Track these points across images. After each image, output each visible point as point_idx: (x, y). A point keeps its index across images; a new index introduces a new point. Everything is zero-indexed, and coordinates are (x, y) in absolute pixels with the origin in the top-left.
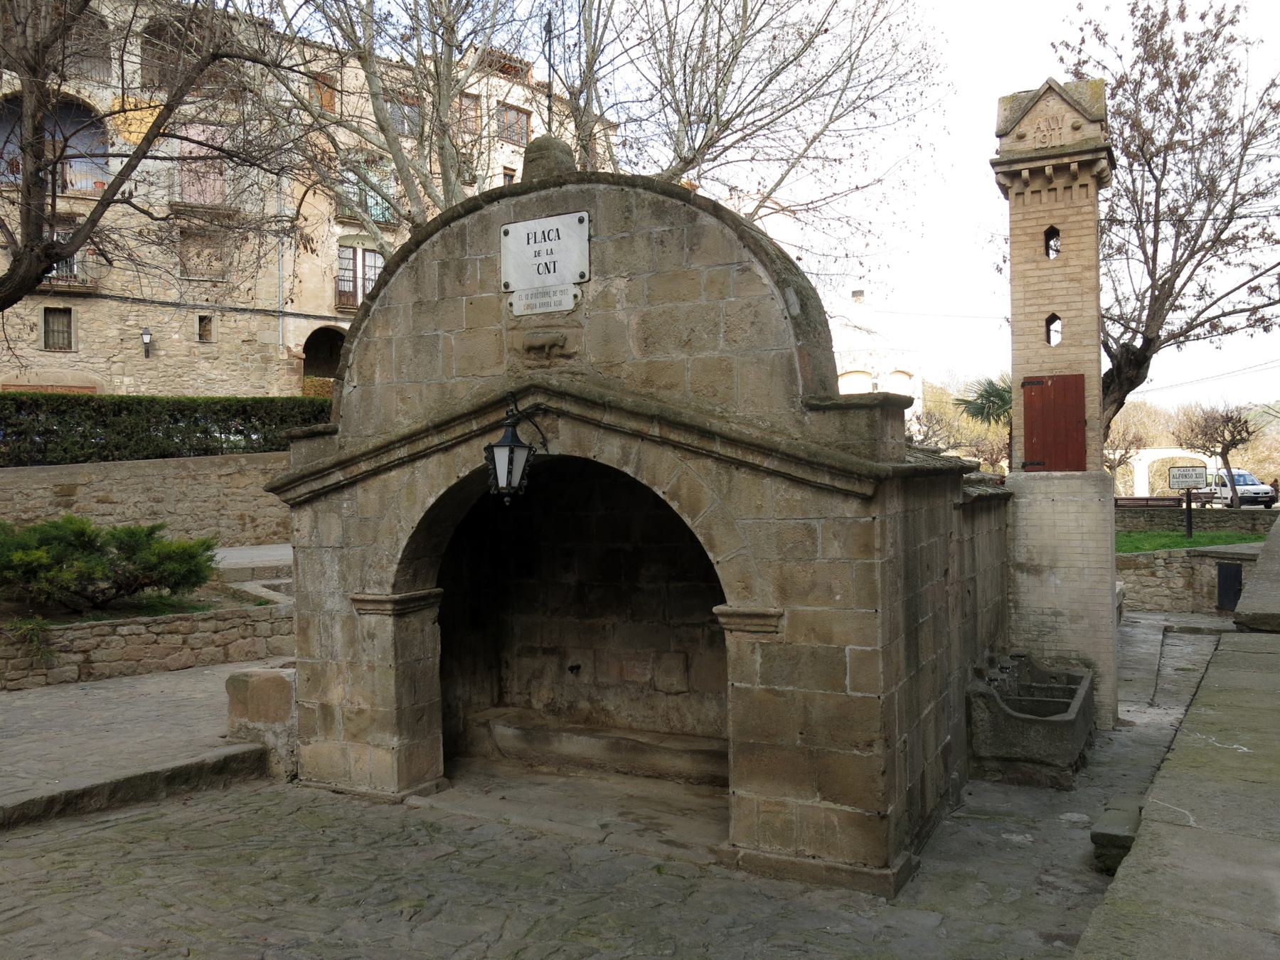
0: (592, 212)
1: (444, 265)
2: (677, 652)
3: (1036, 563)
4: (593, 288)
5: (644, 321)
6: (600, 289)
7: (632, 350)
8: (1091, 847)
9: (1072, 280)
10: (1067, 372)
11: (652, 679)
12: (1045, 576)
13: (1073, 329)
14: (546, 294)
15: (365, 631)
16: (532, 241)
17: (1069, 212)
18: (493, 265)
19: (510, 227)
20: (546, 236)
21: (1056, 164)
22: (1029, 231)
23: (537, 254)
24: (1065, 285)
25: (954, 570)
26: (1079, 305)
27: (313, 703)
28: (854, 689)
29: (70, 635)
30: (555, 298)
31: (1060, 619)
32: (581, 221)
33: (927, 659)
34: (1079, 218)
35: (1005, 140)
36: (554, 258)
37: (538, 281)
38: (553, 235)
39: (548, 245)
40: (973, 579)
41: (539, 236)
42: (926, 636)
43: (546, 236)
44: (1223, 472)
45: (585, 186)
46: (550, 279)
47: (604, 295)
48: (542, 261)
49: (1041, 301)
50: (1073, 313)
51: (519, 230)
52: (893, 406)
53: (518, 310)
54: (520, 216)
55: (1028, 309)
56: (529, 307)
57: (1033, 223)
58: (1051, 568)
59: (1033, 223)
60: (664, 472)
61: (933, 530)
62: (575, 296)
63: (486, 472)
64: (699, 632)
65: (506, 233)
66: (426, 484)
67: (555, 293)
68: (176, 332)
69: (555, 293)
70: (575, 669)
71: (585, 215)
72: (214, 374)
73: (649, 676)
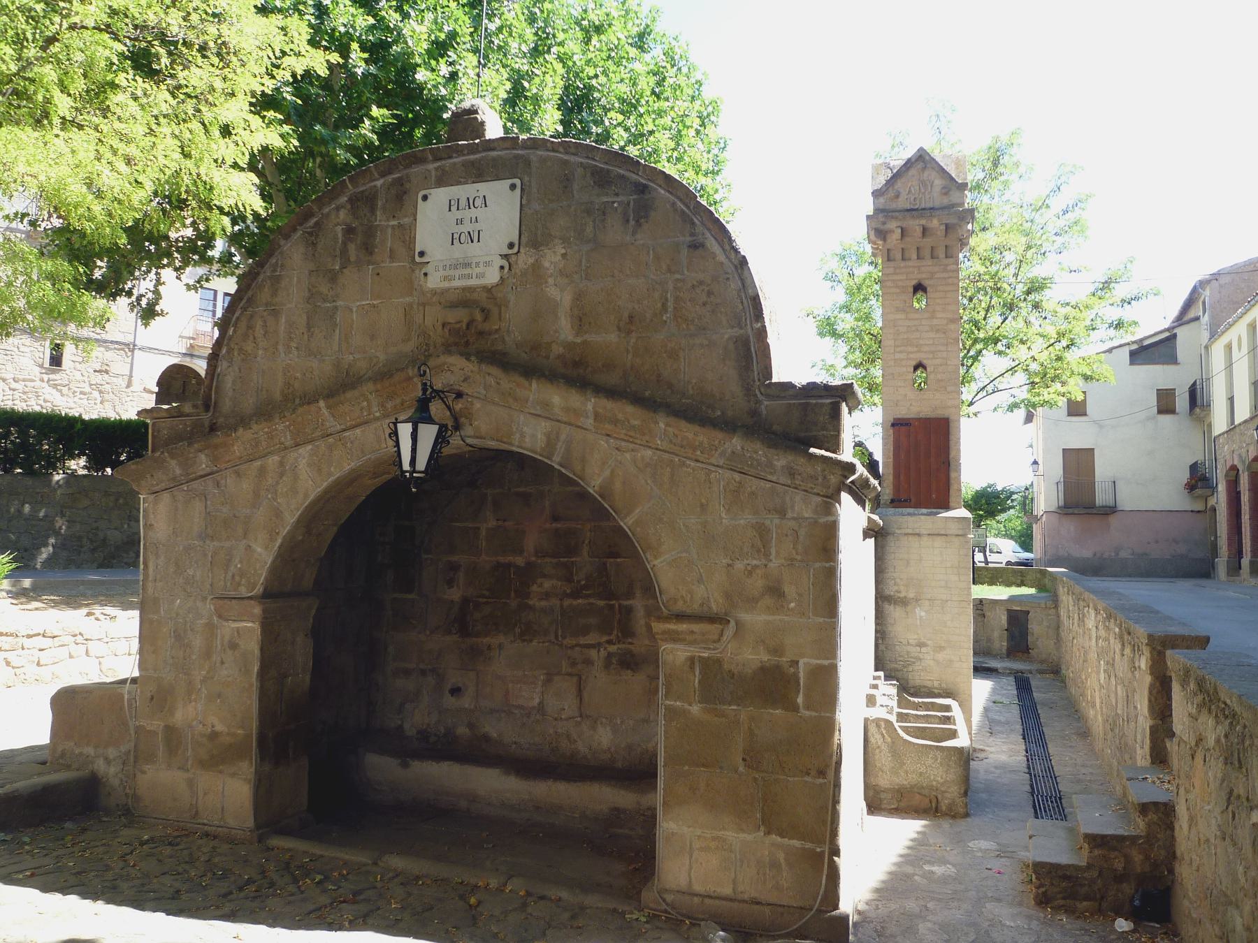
0: (526, 179)
1: (349, 231)
2: (570, 675)
3: (902, 595)
4: (525, 259)
5: (579, 297)
6: (531, 261)
7: (565, 330)
9: (937, 331)
10: (932, 415)
11: (541, 703)
12: (909, 608)
13: (939, 377)
14: (467, 265)
15: (227, 638)
16: (454, 208)
17: (936, 269)
18: (407, 235)
22: (900, 284)
23: (460, 222)
24: (932, 335)
26: (944, 355)
27: (156, 725)
28: (808, 708)
30: (478, 270)
31: (924, 650)
32: (513, 187)
34: (945, 275)
35: (882, 200)
36: (478, 226)
37: (458, 252)
38: (479, 202)
39: (473, 213)
41: (463, 203)
43: (470, 204)
46: (474, 250)
47: (536, 266)
49: (910, 349)
50: (938, 361)
51: (440, 196)
53: (434, 281)
54: (442, 181)
55: (898, 356)
56: (445, 278)
57: (904, 277)
58: (917, 600)
59: (904, 277)
62: (502, 267)
64: (593, 653)
65: (425, 198)
67: (477, 264)
69: (477, 264)
70: (456, 691)
71: (517, 182)
73: (537, 701)
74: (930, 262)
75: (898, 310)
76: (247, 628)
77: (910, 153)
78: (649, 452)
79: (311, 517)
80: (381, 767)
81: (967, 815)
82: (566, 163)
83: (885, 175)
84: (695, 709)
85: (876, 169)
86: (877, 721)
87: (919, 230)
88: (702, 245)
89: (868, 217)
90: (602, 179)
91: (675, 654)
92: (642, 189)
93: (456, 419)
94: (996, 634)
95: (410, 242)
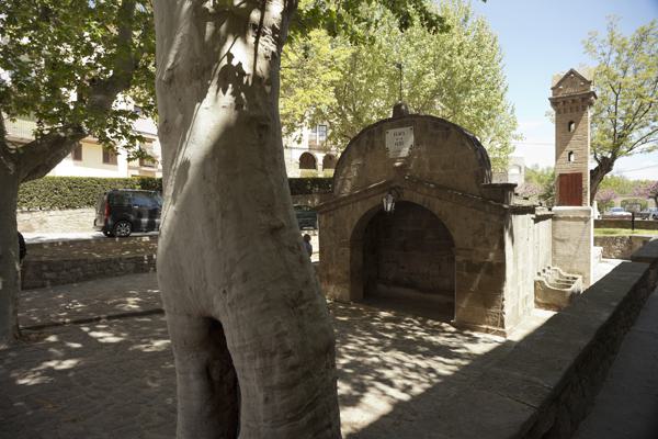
1: (368, 142)
18: (383, 142)
21: (571, 101)
33: (520, 267)
42: (520, 259)
48: (402, 145)
51: (391, 132)
54: (392, 127)
60: (439, 207)
70: (403, 267)
76: (347, 250)
79: (361, 220)
80: (382, 288)
83: (556, 82)
85: (554, 78)
90: (436, 126)
91: (459, 259)
92: (447, 129)
95: (384, 144)
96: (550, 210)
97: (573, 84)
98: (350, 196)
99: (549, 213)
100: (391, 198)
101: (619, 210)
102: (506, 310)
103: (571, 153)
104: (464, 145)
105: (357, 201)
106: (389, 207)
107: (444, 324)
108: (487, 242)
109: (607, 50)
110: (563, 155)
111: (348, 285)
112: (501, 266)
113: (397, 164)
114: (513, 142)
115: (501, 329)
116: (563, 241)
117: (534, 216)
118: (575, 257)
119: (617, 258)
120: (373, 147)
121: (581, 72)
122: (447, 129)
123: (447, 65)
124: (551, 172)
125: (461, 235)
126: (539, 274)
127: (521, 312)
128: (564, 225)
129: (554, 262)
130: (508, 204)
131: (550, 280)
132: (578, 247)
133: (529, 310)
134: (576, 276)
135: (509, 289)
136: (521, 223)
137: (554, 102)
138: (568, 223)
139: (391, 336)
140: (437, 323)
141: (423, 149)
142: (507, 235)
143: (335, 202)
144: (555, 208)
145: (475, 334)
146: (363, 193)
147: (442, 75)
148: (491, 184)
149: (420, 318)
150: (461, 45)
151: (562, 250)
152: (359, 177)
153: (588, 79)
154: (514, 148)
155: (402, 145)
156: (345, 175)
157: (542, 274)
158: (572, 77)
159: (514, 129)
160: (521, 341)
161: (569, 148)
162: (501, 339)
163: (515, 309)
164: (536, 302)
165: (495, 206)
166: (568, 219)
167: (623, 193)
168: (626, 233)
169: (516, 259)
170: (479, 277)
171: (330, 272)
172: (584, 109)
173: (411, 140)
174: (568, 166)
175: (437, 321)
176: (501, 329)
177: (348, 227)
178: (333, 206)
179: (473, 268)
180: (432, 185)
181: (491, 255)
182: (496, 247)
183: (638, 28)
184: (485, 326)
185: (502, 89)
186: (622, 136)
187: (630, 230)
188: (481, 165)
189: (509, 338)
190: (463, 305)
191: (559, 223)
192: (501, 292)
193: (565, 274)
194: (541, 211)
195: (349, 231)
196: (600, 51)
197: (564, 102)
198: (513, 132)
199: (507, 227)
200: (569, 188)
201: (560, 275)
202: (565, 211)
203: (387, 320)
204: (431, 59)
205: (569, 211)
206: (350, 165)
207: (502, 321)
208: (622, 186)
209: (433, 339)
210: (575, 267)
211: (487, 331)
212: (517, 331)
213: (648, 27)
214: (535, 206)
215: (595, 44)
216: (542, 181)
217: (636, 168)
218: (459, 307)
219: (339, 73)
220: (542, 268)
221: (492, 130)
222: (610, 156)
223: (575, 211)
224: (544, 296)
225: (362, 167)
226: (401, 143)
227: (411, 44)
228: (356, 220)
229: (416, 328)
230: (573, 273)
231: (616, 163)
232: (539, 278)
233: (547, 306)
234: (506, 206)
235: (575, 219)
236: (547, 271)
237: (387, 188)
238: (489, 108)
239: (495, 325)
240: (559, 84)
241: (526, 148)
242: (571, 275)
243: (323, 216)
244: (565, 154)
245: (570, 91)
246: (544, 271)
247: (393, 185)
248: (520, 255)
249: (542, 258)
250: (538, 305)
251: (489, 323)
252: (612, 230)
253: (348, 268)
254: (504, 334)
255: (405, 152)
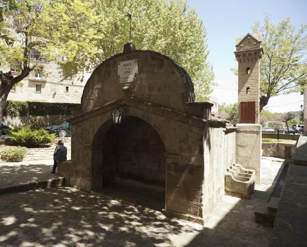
1: (105, 72)
8: (254, 216)
18: (116, 72)
19: (120, 63)
20: (128, 65)
21: (248, 54)
25: (223, 145)
29: (30, 151)
32: (136, 61)
33: (215, 167)
40: (228, 148)
42: (215, 161)
43: (128, 65)
44: (71, 177)
45: (137, 53)
48: (130, 73)
51: (122, 63)
52: (209, 106)
54: (122, 61)
60: (155, 120)
61: (218, 136)
63: (112, 120)
66: (99, 122)
68: (61, 89)
70: (134, 164)
72: (68, 98)
74: (251, 62)
75: (242, 75)
76: (89, 153)
77: (245, 35)
78: (163, 118)
81: (249, 199)
82: (146, 55)
83: (239, 42)
84: (173, 173)
85: (237, 39)
86: (228, 176)
87: (248, 54)
88: (174, 72)
89: (235, 53)
90: (154, 59)
92: (162, 60)
93: (126, 111)
94: (282, 152)
96: (235, 126)
97: (249, 43)
98: (92, 111)
99: (235, 128)
100: (118, 113)
101: (268, 128)
102: (205, 203)
103: (248, 88)
104: (173, 72)
105: (97, 115)
106: (117, 119)
107: (158, 212)
108: (190, 148)
109: (265, 33)
110: (243, 90)
111: (89, 178)
112: (201, 168)
113: (126, 87)
114: (212, 87)
115: (200, 218)
116: (243, 147)
117: (225, 129)
118: (251, 158)
119: (271, 156)
120: (109, 75)
121: (254, 36)
122: (162, 60)
123: (173, 34)
124: (232, 107)
125: (171, 143)
126: (228, 170)
127: (215, 200)
128: (244, 136)
129: (237, 160)
130: (206, 118)
131: (235, 174)
132: (252, 151)
133: (221, 198)
134: (251, 171)
135: (206, 186)
136: (216, 134)
137: (238, 55)
138: (246, 134)
139: (106, 228)
140: (152, 211)
141: (144, 76)
142: (205, 143)
143: (81, 116)
144: (238, 125)
145: (180, 222)
146: (101, 110)
147: (169, 40)
148: (194, 103)
149: (140, 206)
150: (181, 23)
151: (242, 152)
152: (99, 97)
153: (259, 41)
154: (213, 90)
155: (130, 73)
156: (90, 96)
157: (230, 170)
158: (248, 39)
159: (212, 79)
160: (216, 227)
161: (247, 85)
162: (199, 227)
163: (211, 200)
164: (226, 190)
165: (196, 120)
166: (246, 132)
167: (269, 119)
168: (274, 141)
169: (212, 161)
170: (184, 176)
171: (78, 168)
172: (256, 60)
173: (135, 69)
174: (246, 97)
175: (152, 208)
176: (200, 218)
177: (91, 136)
178: (81, 119)
179: (179, 169)
180: (150, 104)
181: (193, 159)
182: (197, 152)
183: (281, 22)
184: (187, 215)
185: (206, 53)
186: (273, 83)
187: (276, 140)
188: (186, 88)
189: (206, 225)
190: (171, 197)
191: (241, 135)
192: (200, 188)
193: (244, 169)
194: (229, 126)
195: (91, 138)
196: (260, 33)
197: (244, 55)
198: (212, 81)
199: (205, 138)
200: (247, 112)
201: (241, 170)
202: (244, 126)
203: (115, 208)
204: (162, 29)
205: (247, 127)
206: (93, 89)
207: (201, 211)
208: (269, 116)
209: (144, 229)
210: (250, 164)
211: (189, 219)
212: (211, 220)
213: (286, 20)
214: (226, 122)
215: (258, 29)
216: (227, 112)
217: (285, 102)
218: (168, 199)
219: (103, 35)
220: (231, 167)
221: (200, 79)
222: (266, 95)
223: (250, 127)
224: (234, 187)
225: (101, 90)
226: (129, 72)
227: (150, 20)
228: (96, 130)
229: (134, 217)
230: (249, 168)
231: (270, 100)
232: (228, 173)
233: (233, 194)
234: (204, 120)
235: (251, 132)
236: (233, 167)
237: (116, 106)
238: (198, 64)
239: (195, 214)
240: (241, 43)
241: (220, 88)
242: (248, 170)
243: (75, 127)
244: (244, 89)
245: (248, 48)
246: (231, 168)
247: (122, 104)
248: (215, 157)
249: (230, 159)
250: (227, 192)
251: (190, 213)
252: (266, 139)
253: (90, 165)
254: (201, 222)
255: (131, 78)
